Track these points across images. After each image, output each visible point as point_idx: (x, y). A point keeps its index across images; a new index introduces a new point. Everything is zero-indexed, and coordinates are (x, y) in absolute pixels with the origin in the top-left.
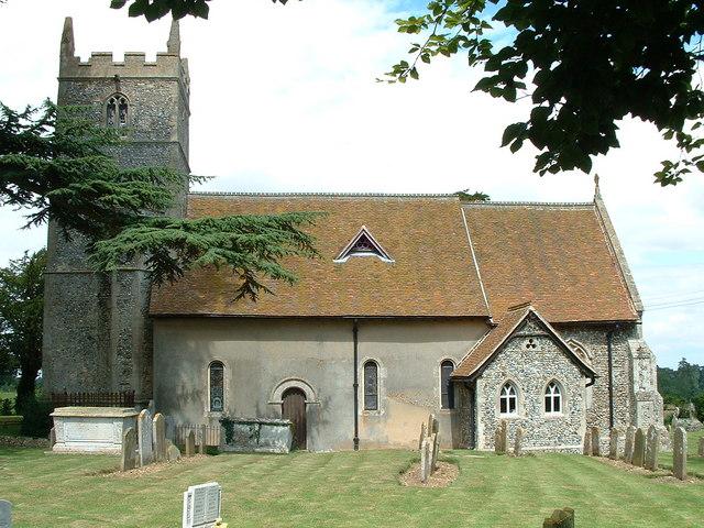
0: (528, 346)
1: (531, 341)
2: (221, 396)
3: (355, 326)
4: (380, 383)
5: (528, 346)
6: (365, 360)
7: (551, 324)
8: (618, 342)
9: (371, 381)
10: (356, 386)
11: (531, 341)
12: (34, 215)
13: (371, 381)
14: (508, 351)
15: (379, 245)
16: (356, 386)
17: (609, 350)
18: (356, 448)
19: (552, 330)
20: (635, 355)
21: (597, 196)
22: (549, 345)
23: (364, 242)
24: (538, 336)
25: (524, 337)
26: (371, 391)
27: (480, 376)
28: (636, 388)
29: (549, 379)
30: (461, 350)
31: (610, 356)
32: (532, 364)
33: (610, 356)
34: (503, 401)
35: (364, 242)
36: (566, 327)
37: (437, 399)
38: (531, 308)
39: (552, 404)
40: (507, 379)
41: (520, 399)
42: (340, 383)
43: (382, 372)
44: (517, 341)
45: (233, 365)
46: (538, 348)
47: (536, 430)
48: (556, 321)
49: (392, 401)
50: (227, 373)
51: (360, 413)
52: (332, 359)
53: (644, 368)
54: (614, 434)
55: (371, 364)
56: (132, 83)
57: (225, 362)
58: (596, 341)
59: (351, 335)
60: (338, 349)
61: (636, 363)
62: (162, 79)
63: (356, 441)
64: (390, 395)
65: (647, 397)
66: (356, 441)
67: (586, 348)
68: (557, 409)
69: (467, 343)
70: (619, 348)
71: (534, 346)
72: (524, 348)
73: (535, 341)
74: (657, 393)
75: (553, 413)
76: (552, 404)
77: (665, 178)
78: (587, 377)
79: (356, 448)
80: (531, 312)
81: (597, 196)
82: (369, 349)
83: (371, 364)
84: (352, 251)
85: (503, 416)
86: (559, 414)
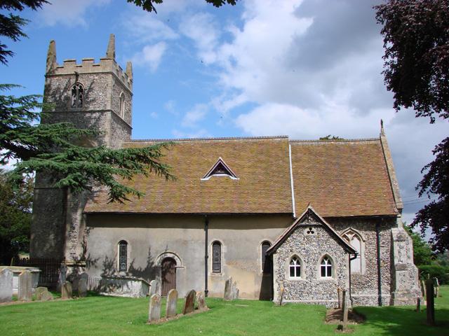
0: (308, 232)
1: (311, 229)
2: (126, 262)
3: (206, 220)
4: (222, 255)
5: (308, 232)
6: (212, 241)
7: (323, 218)
8: (385, 229)
9: (217, 254)
10: (206, 257)
11: (311, 229)
12: (4, 154)
13: (217, 254)
14: (295, 235)
15: (230, 168)
16: (206, 257)
17: (377, 235)
18: (206, 296)
19: (325, 222)
20: (395, 239)
21: (382, 134)
22: (323, 234)
23: (220, 168)
24: (315, 226)
25: (305, 227)
26: (217, 260)
27: (275, 252)
28: (396, 262)
29: (323, 254)
30: (274, 234)
31: (378, 239)
32: (311, 244)
33: (378, 239)
34: (292, 269)
35: (220, 168)
36: (333, 220)
37: (258, 268)
38: (310, 207)
39: (326, 271)
40: (294, 254)
41: (304, 266)
42: (197, 255)
43: (224, 249)
44: (300, 230)
45: (132, 243)
46: (316, 234)
47: (314, 289)
48: (332, 214)
49: (230, 267)
50: (129, 248)
51: (209, 274)
52: (192, 240)
53: (401, 248)
54: (103, 305)
55: (217, 244)
56: (84, 76)
57: (221, 241)
58: (369, 229)
59: (204, 224)
60: (196, 234)
61: (395, 244)
62: (103, 73)
63: (206, 292)
64: (228, 263)
65: (403, 267)
66: (206, 292)
67: (361, 234)
68: (329, 274)
69: (281, 230)
70: (384, 234)
71: (313, 232)
72: (306, 234)
73: (313, 229)
74: (413, 265)
75: (327, 278)
76: (326, 271)
77: (433, 121)
78: (350, 253)
79: (206, 296)
80: (309, 209)
81: (382, 134)
82: (215, 234)
83: (217, 244)
84: (213, 173)
85: (292, 278)
86: (299, 278)
